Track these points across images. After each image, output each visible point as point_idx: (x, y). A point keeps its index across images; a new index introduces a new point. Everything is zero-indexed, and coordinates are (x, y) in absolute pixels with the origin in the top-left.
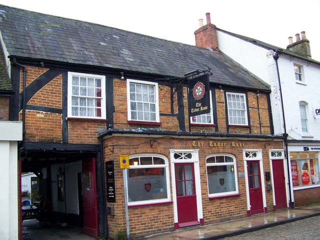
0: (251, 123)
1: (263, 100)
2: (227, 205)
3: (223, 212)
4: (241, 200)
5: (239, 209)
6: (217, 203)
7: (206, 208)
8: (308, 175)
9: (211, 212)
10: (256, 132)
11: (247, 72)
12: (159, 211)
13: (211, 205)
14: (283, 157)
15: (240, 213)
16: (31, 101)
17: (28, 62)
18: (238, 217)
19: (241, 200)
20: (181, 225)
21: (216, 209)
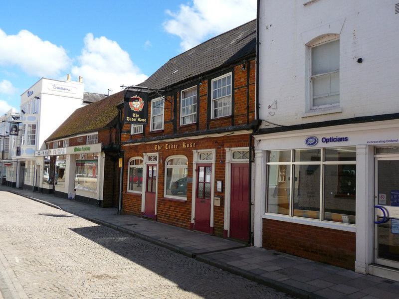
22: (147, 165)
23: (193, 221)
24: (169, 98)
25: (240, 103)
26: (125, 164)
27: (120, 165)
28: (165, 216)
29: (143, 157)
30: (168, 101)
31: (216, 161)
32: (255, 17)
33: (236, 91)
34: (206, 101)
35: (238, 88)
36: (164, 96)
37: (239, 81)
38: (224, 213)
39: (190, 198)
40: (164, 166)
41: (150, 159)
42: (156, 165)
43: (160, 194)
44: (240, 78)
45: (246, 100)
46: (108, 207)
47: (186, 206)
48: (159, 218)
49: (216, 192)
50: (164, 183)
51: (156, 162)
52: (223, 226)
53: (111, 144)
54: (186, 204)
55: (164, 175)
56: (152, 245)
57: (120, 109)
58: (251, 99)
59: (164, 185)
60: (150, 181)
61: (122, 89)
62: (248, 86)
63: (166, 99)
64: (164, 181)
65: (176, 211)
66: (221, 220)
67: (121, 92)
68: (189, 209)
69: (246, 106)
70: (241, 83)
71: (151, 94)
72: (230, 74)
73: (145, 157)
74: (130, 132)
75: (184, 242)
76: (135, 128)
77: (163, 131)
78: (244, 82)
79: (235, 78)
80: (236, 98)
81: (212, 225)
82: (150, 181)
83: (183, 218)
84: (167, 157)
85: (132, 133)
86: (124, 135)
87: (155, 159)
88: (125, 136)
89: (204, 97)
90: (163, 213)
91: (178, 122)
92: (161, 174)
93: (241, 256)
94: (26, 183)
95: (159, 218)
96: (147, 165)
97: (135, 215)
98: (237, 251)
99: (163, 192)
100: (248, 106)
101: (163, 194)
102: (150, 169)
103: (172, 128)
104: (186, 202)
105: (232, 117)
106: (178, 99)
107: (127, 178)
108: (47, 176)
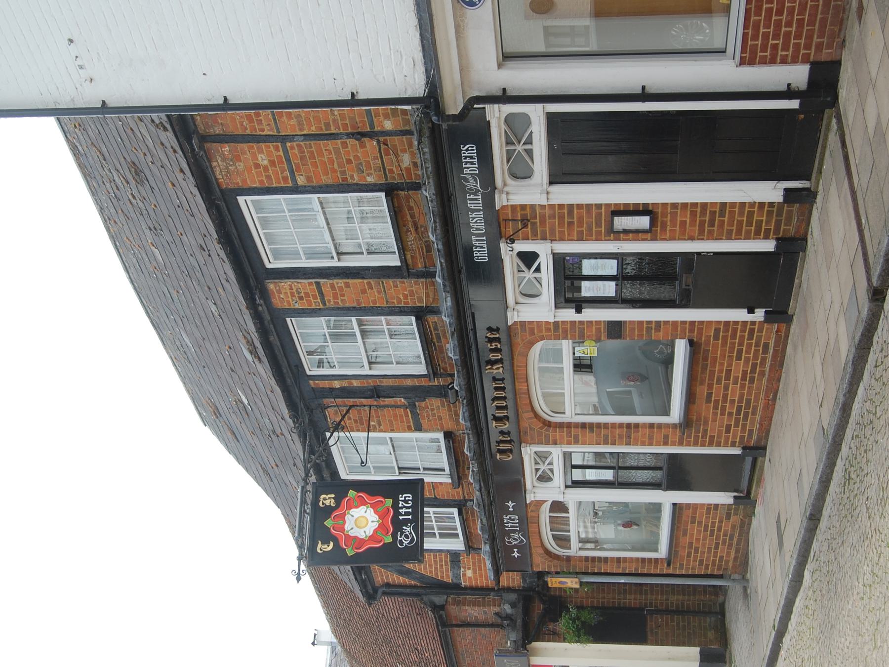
0: (370, 180)
1: (400, 466)
2: (719, 381)
3: (742, 395)
4: (716, 337)
5: (749, 346)
6: (705, 409)
7: (712, 437)
8: (566, 510)
9: (728, 428)
10: (406, 160)
11: (101, 210)
12: (693, 522)
13: (706, 423)
14: (537, 114)
15: (766, 346)
16: (369, 283)
17: (161, 334)
18: (775, 351)
19: (716, 337)
20: (744, 485)
21: (723, 414)
22: (567, 487)
23: (759, 314)
24: (332, 415)
25: (341, 165)
26: (568, 566)
27: (572, 583)
28: (746, 416)
29: (540, 503)
30: (343, 417)
31: (544, 238)
32: (51, 121)
33: (301, 181)
34: (340, 282)
35: (292, 172)
36: (328, 434)
37: (266, 169)
38: (723, 205)
39: (676, 327)
40: (569, 425)
41: (544, 478)
42: (567, 456)
43: (666, 437)
44: (257, 166)
45: (330, 144)
46: (726, 641)
47: (708, 342)
48: (755, 437)
49: (650, 234)
50: (629, 426)
51: (556, 453)
52: (771, 204)
53: (501, 622)
54: (700, 345)
55: (599, 425)
56: (844, 449)
57: (375, 590)
58: (327, 125)
59: (637, 426)
60: (625, 475)
61: (306, 579)
62: (284, 139)
63: (338, 427)
64: (621, 425)
65: (728, 378)
66: (751, 214)
67: (315, 582)
68: (717, 331)
69: (351, 142)
70: (272, 163)
71: (320, 477)
72: (240, 199)
73: (539, 497)
74: (455, 556)
75: (832, 342)
76: (400, 473)
77: (448, 435)
78: (269, 154)
79: (257, 185)
80: (326, 180)
81: (768, 246)
82: (625, 475)
83: (748, 352)
84: (536, 415)
85: (458, 545)
86: (469, 575)
87: (542, 457)
88: (469, 573)
89: (327, 290)
90: (737, 425)
91: (416, 382)
92: (599, 435)
93: (871, 130)
94: (100, 106)
95: (755, 437)
96: (567, 487)
97: (745, 527)
98: (855, 141)
99: (660, 426)
100: (351, 135)
101: (667, 426)
102: (577, 475)
103: (435, 402)
104: (691, 343)
105: (391, 191)
106: (337, 384)
107: (618, 560)
108: (260, 308)
